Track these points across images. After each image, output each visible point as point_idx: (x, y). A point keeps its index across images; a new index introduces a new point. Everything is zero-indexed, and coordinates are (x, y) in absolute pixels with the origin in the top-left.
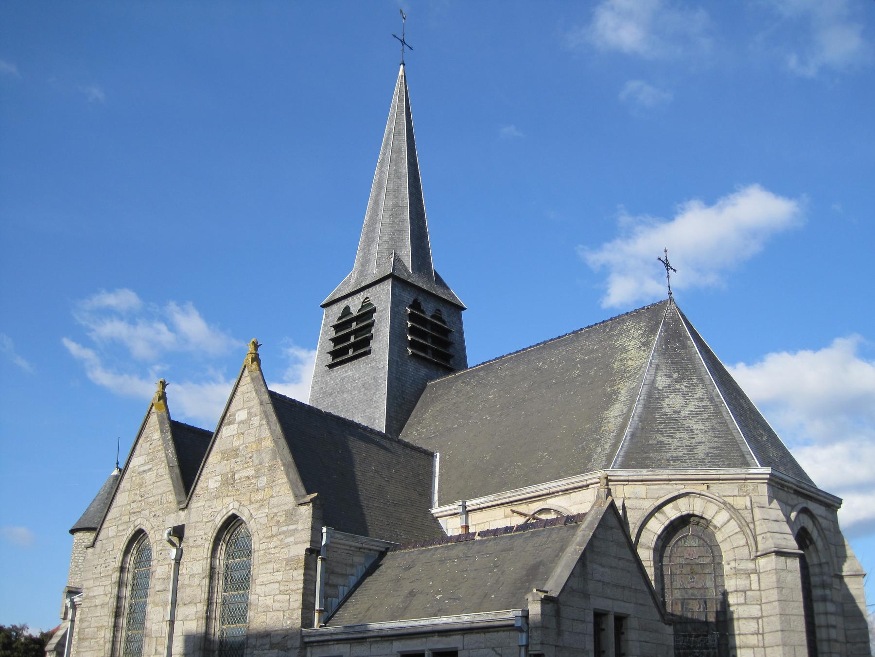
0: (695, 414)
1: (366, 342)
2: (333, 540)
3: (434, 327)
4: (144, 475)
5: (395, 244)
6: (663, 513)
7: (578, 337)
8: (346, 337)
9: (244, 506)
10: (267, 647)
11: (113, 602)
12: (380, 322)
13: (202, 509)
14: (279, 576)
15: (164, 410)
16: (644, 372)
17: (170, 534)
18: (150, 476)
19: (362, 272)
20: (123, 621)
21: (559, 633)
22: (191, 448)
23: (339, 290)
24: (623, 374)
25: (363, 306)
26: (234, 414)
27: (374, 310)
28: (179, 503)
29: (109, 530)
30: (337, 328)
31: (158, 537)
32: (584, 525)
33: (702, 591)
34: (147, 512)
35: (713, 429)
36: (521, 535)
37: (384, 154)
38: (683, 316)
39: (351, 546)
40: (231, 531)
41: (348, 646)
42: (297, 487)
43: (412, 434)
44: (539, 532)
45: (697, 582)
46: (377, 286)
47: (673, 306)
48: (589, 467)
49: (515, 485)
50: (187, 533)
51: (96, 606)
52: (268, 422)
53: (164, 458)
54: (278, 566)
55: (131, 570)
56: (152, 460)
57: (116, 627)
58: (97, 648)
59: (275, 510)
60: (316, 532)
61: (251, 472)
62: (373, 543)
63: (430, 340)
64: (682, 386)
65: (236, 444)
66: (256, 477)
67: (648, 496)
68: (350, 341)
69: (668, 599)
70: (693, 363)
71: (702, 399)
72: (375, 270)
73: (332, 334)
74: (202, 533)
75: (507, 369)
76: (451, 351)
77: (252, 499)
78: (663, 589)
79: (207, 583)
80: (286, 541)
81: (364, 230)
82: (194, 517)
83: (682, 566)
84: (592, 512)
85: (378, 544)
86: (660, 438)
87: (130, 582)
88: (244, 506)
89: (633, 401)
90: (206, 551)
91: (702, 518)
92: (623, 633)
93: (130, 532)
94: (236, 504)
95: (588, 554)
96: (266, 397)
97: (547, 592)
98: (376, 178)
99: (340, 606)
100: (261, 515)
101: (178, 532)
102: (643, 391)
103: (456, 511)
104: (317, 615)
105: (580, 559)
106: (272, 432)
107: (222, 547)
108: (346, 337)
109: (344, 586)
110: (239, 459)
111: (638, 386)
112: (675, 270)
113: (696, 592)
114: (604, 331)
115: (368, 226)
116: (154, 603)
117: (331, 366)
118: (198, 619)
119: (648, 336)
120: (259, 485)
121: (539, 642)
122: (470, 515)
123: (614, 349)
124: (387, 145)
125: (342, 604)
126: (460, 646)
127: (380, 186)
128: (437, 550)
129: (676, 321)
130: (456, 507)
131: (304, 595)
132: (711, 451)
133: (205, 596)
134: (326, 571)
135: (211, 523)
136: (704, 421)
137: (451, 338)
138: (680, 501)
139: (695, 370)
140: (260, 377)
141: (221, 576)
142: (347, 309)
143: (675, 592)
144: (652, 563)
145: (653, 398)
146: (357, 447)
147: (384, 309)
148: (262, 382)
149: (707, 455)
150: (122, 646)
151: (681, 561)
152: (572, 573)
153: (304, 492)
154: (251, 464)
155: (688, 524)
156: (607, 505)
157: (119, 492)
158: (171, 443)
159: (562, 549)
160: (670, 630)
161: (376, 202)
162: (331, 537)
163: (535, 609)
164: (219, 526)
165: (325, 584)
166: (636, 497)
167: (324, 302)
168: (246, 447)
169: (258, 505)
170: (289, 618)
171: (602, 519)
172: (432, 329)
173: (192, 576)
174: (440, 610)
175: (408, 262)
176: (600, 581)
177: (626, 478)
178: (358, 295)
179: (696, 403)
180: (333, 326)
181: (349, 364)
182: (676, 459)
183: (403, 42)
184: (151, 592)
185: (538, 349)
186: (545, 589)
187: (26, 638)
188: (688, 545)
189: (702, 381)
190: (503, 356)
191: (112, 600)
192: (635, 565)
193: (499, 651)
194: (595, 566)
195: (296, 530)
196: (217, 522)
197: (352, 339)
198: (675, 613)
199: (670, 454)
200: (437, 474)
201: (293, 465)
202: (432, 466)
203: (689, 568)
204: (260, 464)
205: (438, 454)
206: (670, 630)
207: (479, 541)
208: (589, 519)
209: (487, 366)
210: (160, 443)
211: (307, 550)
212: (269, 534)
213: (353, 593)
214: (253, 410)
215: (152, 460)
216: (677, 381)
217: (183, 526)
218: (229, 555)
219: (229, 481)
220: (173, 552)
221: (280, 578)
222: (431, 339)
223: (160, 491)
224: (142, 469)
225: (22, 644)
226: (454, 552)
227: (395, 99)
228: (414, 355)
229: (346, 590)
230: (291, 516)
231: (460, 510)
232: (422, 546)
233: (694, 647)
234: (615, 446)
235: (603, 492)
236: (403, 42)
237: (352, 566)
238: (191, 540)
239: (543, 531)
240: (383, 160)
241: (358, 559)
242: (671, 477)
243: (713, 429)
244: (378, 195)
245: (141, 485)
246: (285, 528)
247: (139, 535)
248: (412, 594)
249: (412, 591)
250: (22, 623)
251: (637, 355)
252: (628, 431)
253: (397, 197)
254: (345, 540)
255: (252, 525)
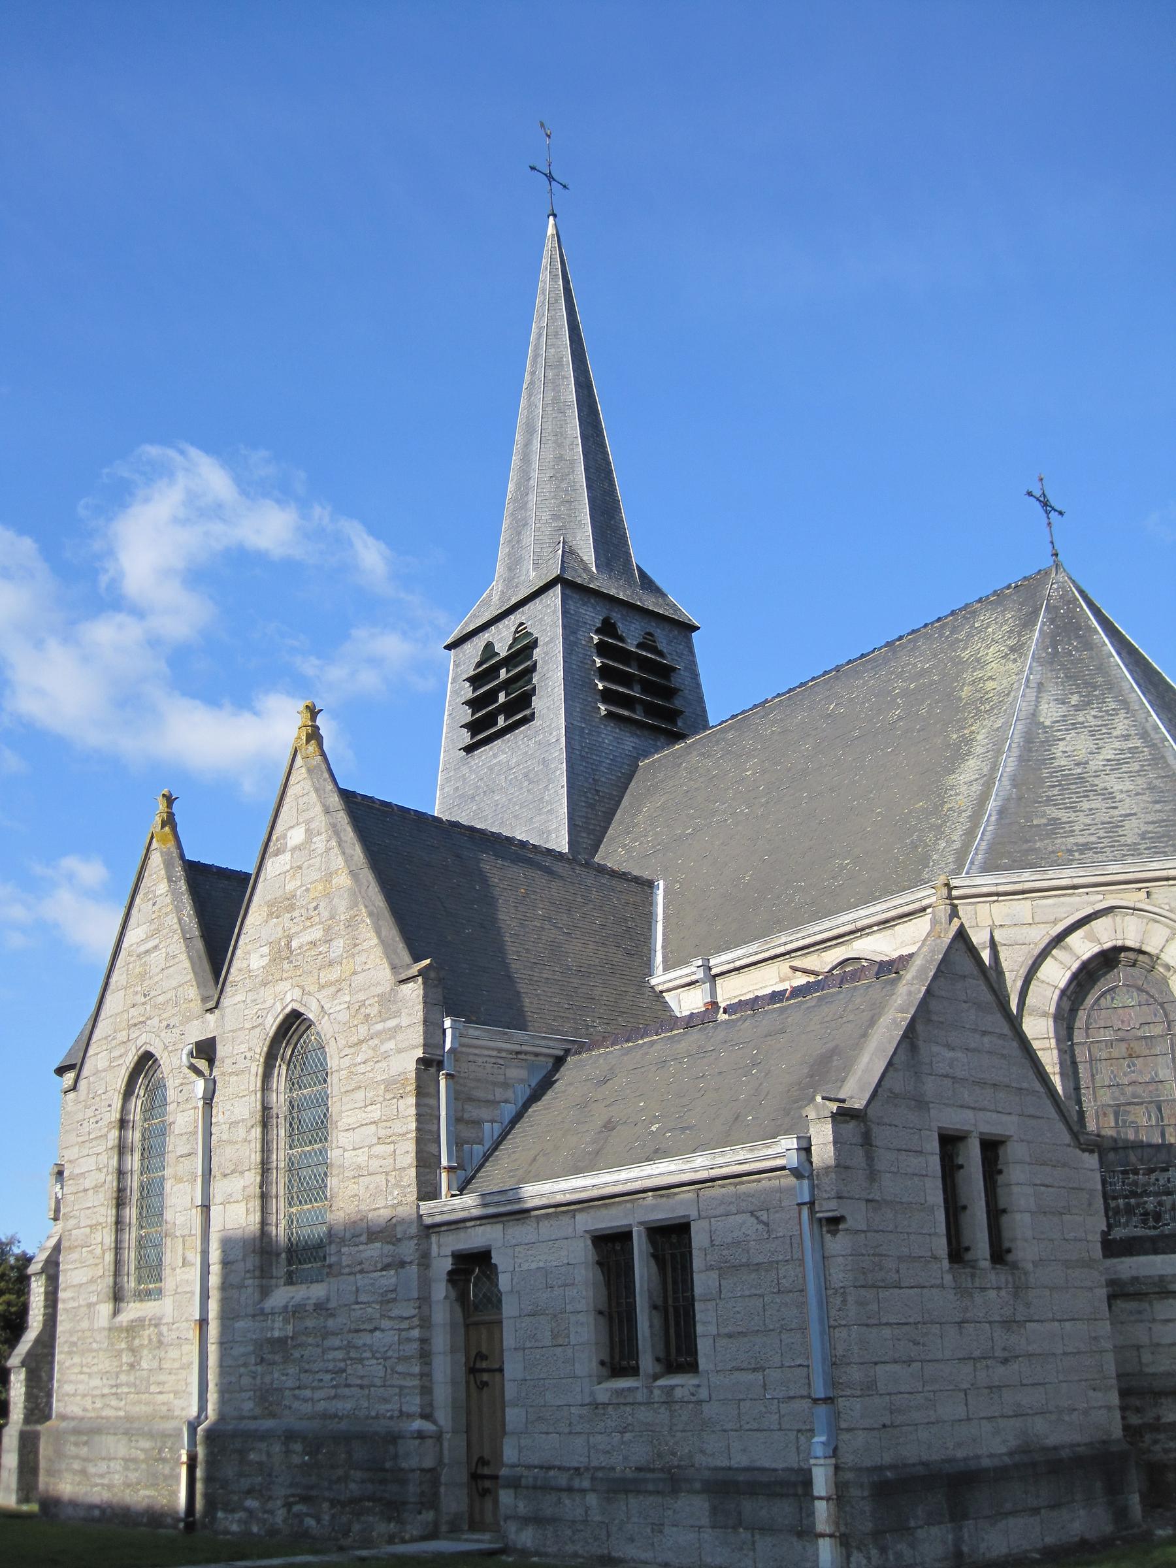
0: (1115, 765)
1: (525, 700)
2: (465, 1040)
3: (644, 663)
4: (147, 959)
5: (563, 524)
6: (1068, 948)
7: (895, 652)
8: (492, 696)
9: (309, 994)
10: (364, 1238)
11: (111, 1181)
12: (546, 663)
13: (242, 1006)
14: (375, 1112)
15: (171, 844)
16: (1016, 698)
17: (191, 1054)
18: (157, 960)
19: (509, 582)
20: (131, 1213)
21: (873, 1175)
22: (217, 902)
23: (474, 616)
24: (980, 706)
25: (515, 639)
26: (284, 837)
27: (534, 644)
28: (205, 999)
29: (97, 1059)
30: (475, 681)
31: (176, 1062)
32: (909, 975)
33: (1151, 1087)
34: (156, 1020)
35: (1151, 788)
36: (799, 1004)
37: (533, 373)
38: (1081, 592)
39: (500, 1050)
40: (293, 1041)
41: (500, 1227)
42: (395, 952)
43: (614, 853)
44: (832, 995)
45: (1141, 1072)
46: (537, 601)
47: (1062, 577)
48: (925, 876)
49: (795, 922)
50: (221, 1051)
51: (86, 1190)
52: (340, 843)
53: (177, 926)
54: (370, 1095)
55: (138, 1124)
56: (158, 931)
57: (118, 1222)
58: (91, 1261)
59: (361, 996)
60: (432, 1029)
61: (317, 933)
62: (539, 1040)
63: (637, 687)
64: (1089, 717)
65: (290, 887)
66: (326, 942)
67: (1037, 920)
68: (498, 702)
69: (1089, 1106)
70: (1106, 674)
71: (1126, 737)
72: (532, 575)
73: (468, 693)
74: (244, 1048)
75: (774, 723)
76: (678, 703)
77: (323, 981)
78: (1077, 1089)
79: (259, 1136)
80: (384, 1048)
81: (508, 508)
82: (231, 1023)
83: (1110, 1044)
84: (925, 949)
85: (551, 1044)
86: (1053, 812)
87: (138, 1145)
88: (309, 994)
89: (999, 752)
90: (253, 1078)
91: (1141, 952)
92: (1000, 1172)
93: (131, 1059)
94: (297, 993)
95: (920, 1028)
96: (335, 800)
97: (843, 1101)
98: (521, 417)
99: (486, 1157)
100: (338, 1007)
101: (206, 1050)
102: (1016, 732)
103: (694, 978)
104: (444, 1175)
105: (905, 1036)
106: (348, 859)
107: (281, 1071)
108: (492, 696)
109: (492, 1121)
110: (296, 913)
111: (1007, 724)
112: (1061, 513)
113: (1139, 1089)
114: (941, 636)
115: (514, 500)
116: (175, 1177)
117: (469, 749)
118: (247, 1199)
119: (1020, 635)
120: (332, 955)
121: (833, 1194)
122: (719, 981)
123: (960, 663)
124: (536, 357)
125: (490, 1155)
126: (694, 1214)
127: (530, 429)
128: (653, 1045)
129: (1069, 602)
130: (693, 970)
131: (419, 1141)
132: (1151, 828)
133: (257, 1157)
134: (456, 1096)
135: (258, 1030)
136: (1132, 776)
137: (675, 681)
138: (1096, 924)
139: (1112, 685)
140: (324, 766)
141: (281, 1121)
142: (489, 646)
143: (1102, 1091)
144: (1053, 1041)
145: (1036, 744)
146: (489, 865)
147: (552, 640)
148: (326, 775)
149: (1143, 835)
150: (132, 1255)
151: (1109, 1035)
152: (890, 1064)
153: (406, 958)
154: (316, 919)
155: (1117, 966)
156: (951, 934)
157: (109, 992)
158: (186, 900)
159: (872, 1022)
160: (1092, 1160)
161: (526, 459)
162: (461, 1035)
163: (822, 1137)
164: (271, 1034)
165: (456, 1120)
166: (1013, 924)
167: (449, 641)
168: (308, 890)
169: (333, 989)
170: (396, 1186)
171: (943, 960)
172: (640, 668)
173: (234, 1124)
174: (656, 1151)
175: (588, 554)
176: (946, 1076)
177: (993, 889)
178: (506, 621)
179: (1117, 745)
180: (467, 680)
181: (498, 742)
182: (1085, 848)
183: (550, 177)
184: (170, 1158)
185: (826, 682)
186: (841, 1096)
187: (17, 1258)
188: (1118, 1007)
189: (1125, 704)
190: (766, 701)
191: (109, 1178)
192: (1015, 1044)
193: (764, 1216)
194: (935, 1049)
195: (398, 1027)
196: (268, 1026)
197: (502, 697)
198: (1103, 1133)
199: (1072, 840)
200: (660, 917)
201: (387, 914)
202: (651, 904)
203: (1124, 1046)
204: (332, 917)
205: (661, 883)
206: (1092, 1160)
207: (726, 1021)
208: (918, 962)
209: (740, 720)
210: (169, 900)
211: (419, 1060)
212: (355, 1039)
213: (508, 1133)
214: (313, 825)
215: (158, 931)
216: (1077, 708)
217: (213, 1039)
218: (292, 1084)
219: (282, 953)
220: (200, 1084)
221: (376, 1115)
222: (642, 684)
223: (174, 983)
224: (142, 949)
225: (12, 1268)
226: (683, 1046)
227: (545, 276)
228: (610, 715)
229: (497, 1127)
230: (387, 1002)
231: (700, 974)
232: (627, 1041)
233: (1145, 1193)
234: (970, 834)
235: (943, 910)
236: (550, 177)
237: (506, 1085)
238: (228, 1061)
239: (839, 992)
240: (532, 383)
241: (515, 1073)
242: (1076, 881)
243: (1151, 788)
244: (527, 444)
245: (143, 976)
246: (379, 1027)
247: (146, 1061)
248: (609, 1126)
249: (609, 1122)
250: (10, 1233)
251: (1002, 669)
252: (992, 805)
253: (560, 446)
254: (486, 1039)
255: (324, 1027)
